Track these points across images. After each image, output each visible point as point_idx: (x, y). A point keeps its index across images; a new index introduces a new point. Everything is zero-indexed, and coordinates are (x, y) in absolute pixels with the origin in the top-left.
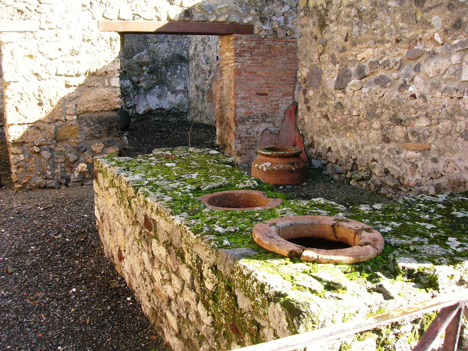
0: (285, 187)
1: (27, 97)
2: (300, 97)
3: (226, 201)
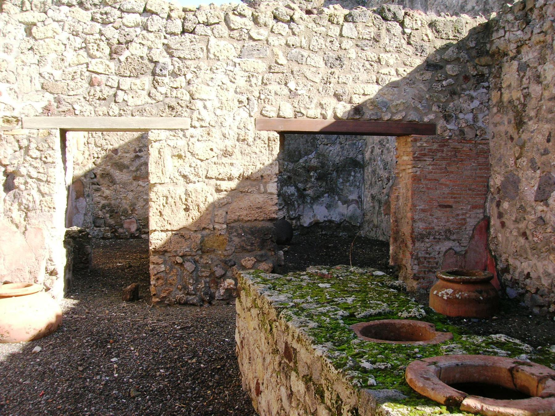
0: (470, 321)
1: (173, 201)
2: (493, 211)
3: (382, 331)
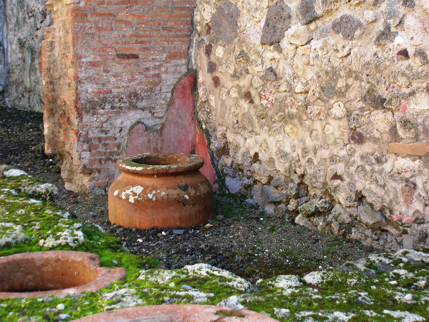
0: (171, 233)
2: (200, 61)
